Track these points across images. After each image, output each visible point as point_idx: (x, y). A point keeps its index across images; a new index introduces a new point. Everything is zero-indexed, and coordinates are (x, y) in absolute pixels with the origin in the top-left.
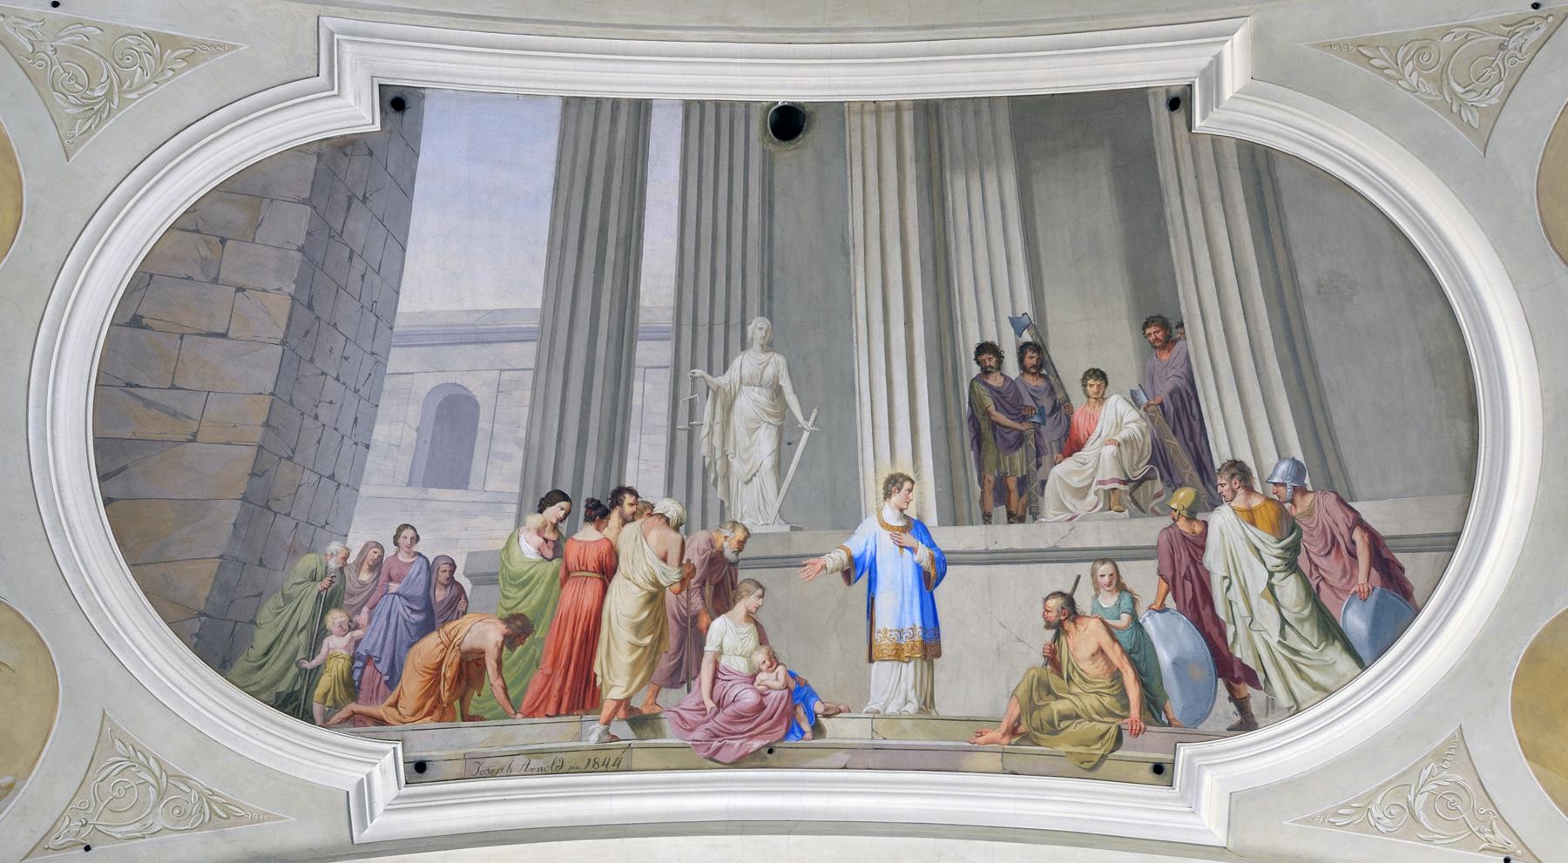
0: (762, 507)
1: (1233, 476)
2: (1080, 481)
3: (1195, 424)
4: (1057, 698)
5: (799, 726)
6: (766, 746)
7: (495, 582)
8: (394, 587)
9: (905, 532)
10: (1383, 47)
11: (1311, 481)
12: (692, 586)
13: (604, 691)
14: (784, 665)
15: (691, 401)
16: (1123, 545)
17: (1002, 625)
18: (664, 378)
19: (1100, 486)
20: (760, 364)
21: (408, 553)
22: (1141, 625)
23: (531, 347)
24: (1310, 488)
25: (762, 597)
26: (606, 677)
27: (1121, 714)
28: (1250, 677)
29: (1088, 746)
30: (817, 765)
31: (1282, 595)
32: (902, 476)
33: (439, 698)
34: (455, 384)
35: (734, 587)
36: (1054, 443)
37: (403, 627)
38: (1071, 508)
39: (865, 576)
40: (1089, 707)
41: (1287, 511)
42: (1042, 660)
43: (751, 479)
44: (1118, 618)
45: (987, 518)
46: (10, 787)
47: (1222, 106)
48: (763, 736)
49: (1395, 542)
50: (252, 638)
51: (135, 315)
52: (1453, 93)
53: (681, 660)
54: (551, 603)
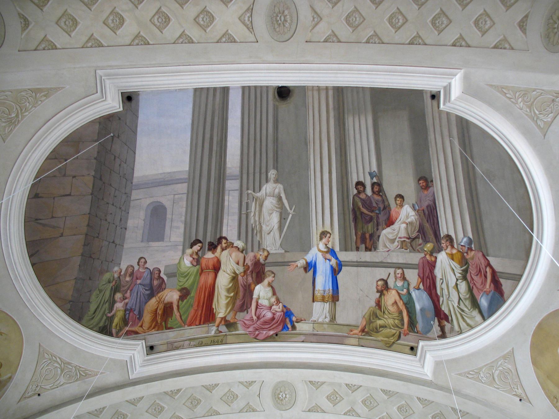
1: (447, 240)
2: (392, 237)
3: (435, 219)
4: (379, 319)
6: (275, 333)
7: (175, 276)
8: (139, 282)
9: (327, 253)
11: (474, 246)
12: (248, 273)
13: (216, 315)
15: (247, 203)
16: (407, 262)
17: (361, 290)
18: (236, 194)
19: (400, 239)
20: (273, 188)
21: (143, 268)
24: (473, 249)
25: (274, 277)
26: (217, 309)
27: (401, 327)
28: (446, 318)
29: (389, 338)
30: (293, 341)
31: (460, 289)
32: (327, 231)
34: (157, 202)
35: (264, 273)
36: (383, 222)
37: (143, 296)
38: (388, 247)
39: (312, 269)
40: (390, 324)
41: (464, 256)
43: (270, 233)
44: (403, 290)
45: (358, 249)
47: (451, 102)
48: (274, 330)
49: (501, 274)
50: (89, 308)
51: (36, 194)
52: (535, 113)
53: (244, 302)
54: (196, 283)
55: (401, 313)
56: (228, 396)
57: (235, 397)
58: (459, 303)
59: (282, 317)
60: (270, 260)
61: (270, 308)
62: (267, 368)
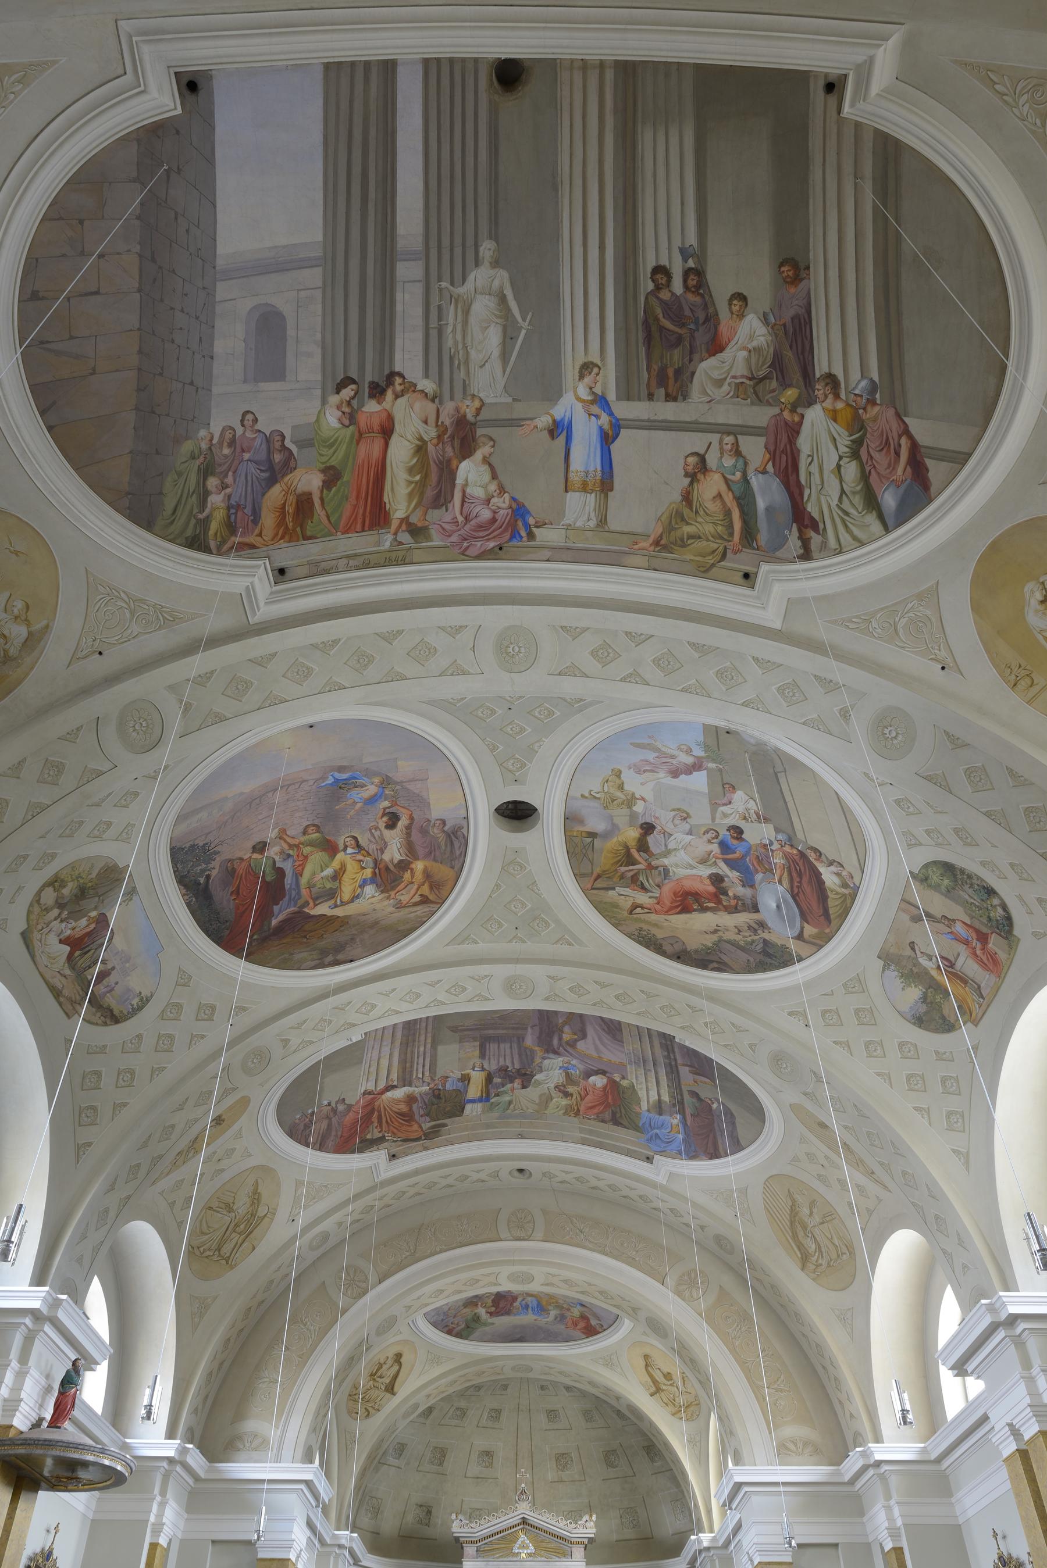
0: (492, 384)
1: (827, 384)
2: (718, 375)
4: (688, 524)
5: (519, 534)
7: (312, 445)
8: (246, 456)
9: (593, 404)
10: (1008, 76)
12: (446, 440)
13: (391, 513)
14: (507, 492)
15: (440, 307)
16: (744, 424)
17: (655, 472)
18: (418, 290)
19: (733, 380)
21: (252, 431)
22: (748, 481)
23: (319, 270)
24: (878, 402)
25: (493, 446)
26: (392, 504)
28: (814, 525)
32: (592, 363)
33: (287, 527)
34: (267, 304)
37: (257, 482)
39: (565, 433)
41: (859, 414)
42: (680, 498)
43: (484, 365)
44: (734, 474)
45: (651, 397)
46: (47, 627)
47: (867, 101)
53: (440, 491)
55: (728, 513)
56: (420, 650)
57: (432, 651)
58: (840, 499)
59: (509, 517)
60: (484, 415)
61: (488, 501)
62: (486, 605)
